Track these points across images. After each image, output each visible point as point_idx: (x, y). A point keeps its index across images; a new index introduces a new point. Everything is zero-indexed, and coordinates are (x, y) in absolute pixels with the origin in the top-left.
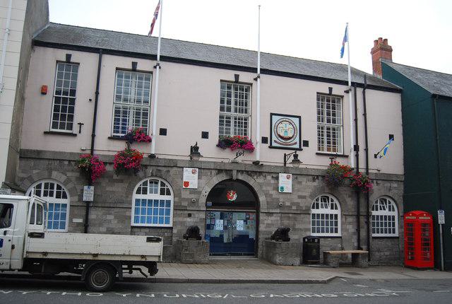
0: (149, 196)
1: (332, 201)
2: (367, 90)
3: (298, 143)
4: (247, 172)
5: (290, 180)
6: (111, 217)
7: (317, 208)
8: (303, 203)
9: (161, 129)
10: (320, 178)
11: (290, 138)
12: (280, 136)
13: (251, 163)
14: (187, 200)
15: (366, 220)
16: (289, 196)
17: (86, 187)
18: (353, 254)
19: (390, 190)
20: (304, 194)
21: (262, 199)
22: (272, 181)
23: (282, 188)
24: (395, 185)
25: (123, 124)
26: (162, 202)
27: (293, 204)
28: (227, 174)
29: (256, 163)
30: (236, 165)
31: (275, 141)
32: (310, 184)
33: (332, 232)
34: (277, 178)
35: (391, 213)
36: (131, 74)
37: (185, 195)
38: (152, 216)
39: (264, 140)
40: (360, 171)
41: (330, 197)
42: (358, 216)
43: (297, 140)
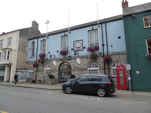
0: (92, 69)
2: (106, 24)
4: (68, 59)
5: (80, 60)
6: (40, 74)
7: (91, 68)
8: (85, 67)
11: (79, 47)
12: (77, 48)
14: (54, 69)
17: (127, 65)
18: (3, 77)
19: (120, 58)
20: (84, 64)
21: (72, 66)
22: (75, 61)
23: (77, 63)
24: (122, 56)
25: (97, 44)
26: (96, 70)
29: (70, 56)
32: (86, 60)
34: (76, 60)
35: (97, 68)
37: (54, 67)
39: (72, 49)
41: (95, 63)
42: (105, 69)
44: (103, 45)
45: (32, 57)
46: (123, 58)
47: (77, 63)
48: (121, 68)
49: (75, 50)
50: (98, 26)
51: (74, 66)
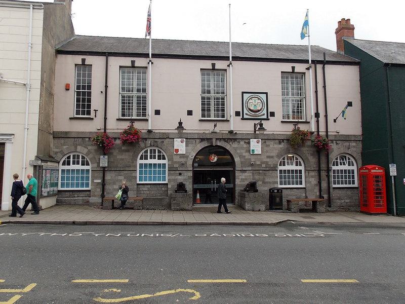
0: (287, 167)
2: (326, 66)
8: (271, 162)
11: (259, 111)
12: (250, 109)
16: (259, 157)
20: (271, 155)
22: (245, 146)
23: (253, 150)
24: (354, 144)
26: (159, 165)
27: (263, 163)
31: (247, 114)
32: (276, 146)
33: (297, 184)
34: (249, 143)
36: (131, 70)
37: (176, 159)
39: (237, 114)
42: (319, 171)
43: (265, 112)
44: (317, 115)
45: (76, 116)
46: (355, 149)
47: (253, 150)
48: (378, 171)
49: (245, 117)
50: (150, 61)
51: (243, 160)
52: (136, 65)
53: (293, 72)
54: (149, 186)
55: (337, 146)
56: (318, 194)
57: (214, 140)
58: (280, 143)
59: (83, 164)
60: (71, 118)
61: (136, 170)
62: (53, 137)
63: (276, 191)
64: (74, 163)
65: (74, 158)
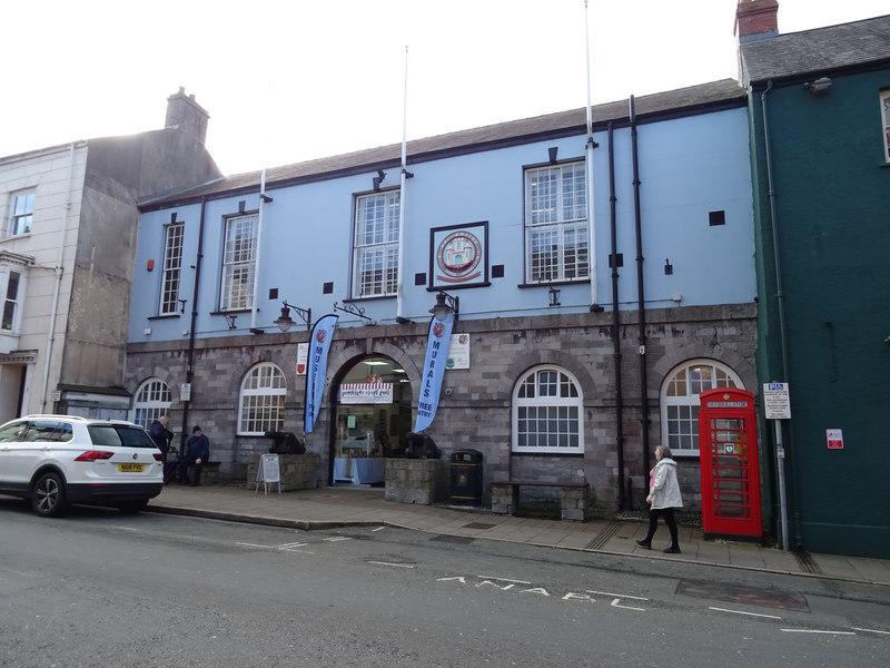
0: (539, 401)
1: (564, 378)
2: (639, 128)
3: (483, 273)
5: (467, 346)
8: (494, 388)
9: (417, 284)
10: (529, 334)
11: (466, 267)
12: (451, 269)
13: (587, 310)
15: (641, 416)
16: (464, 375)
19: (714, 344)
20: (494, 370)
24: (732, 331)
27: (473, 389)
28: (359, 346)
29: (403, 321)
30: (370, 329)
31: (440, 278)
32: (507, 348)
33: (563, 444)
35: (569, 402)
36: (376, 197)
38: (548, 433)
39: (420, 279)
40: (623, 308)
43: (481, 267)
48: (731, 404)
52: (559, 158)
53: (553, 162)
54: (255, 442)
55: (677, 339)
56: (616, 472)
57: (369, 342)
58: (516, 340)
59: (564, 394)
60: (520, 287)
61: (659, 406)
62: (128, 354)
63: (467, 457)
64: (543, 393)
65: (543, 379)
